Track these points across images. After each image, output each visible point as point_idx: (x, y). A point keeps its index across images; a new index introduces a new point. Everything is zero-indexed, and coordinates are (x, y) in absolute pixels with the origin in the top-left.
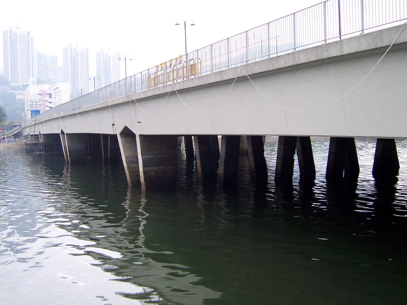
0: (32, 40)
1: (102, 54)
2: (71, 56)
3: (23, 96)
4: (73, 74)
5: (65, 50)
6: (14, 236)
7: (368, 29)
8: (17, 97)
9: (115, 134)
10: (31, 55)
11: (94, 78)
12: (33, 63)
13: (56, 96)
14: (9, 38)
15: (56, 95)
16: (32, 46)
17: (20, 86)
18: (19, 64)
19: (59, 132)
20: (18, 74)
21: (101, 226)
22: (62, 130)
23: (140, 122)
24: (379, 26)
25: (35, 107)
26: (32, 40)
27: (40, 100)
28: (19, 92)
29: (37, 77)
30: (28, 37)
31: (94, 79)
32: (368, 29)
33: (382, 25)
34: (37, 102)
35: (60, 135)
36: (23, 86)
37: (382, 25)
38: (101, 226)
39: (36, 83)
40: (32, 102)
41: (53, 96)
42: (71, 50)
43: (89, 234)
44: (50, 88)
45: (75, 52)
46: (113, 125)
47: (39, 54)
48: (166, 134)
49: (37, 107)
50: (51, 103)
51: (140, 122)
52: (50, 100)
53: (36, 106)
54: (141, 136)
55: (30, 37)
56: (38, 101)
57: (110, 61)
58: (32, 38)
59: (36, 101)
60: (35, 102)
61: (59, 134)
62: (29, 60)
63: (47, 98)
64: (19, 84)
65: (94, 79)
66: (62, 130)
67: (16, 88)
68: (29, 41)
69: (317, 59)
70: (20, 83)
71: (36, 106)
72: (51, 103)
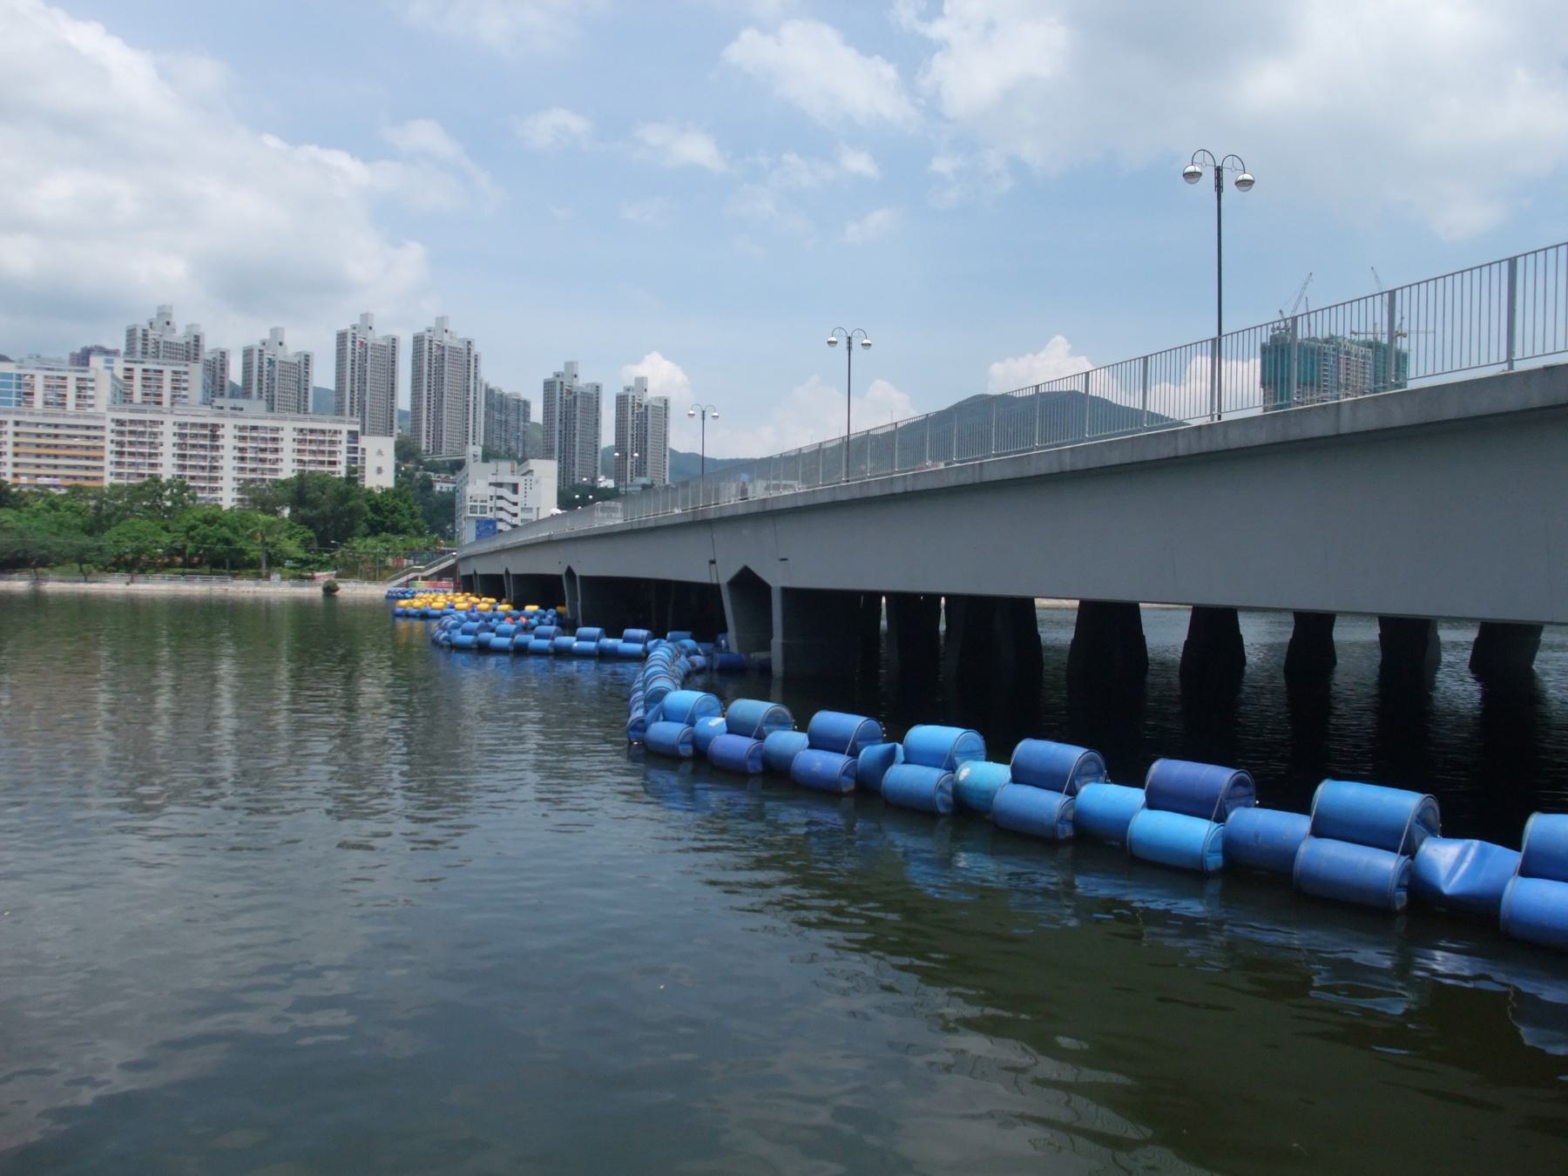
0: (476, 360)
3: (451, 486)
5: (549, 386)
7: (1446, 373)
8: (438, 488)
9: (715, 581)
10: (472, 395)
11: (849, 338)
12: (475, 412)
13: (528, 490)
15: (528, 487)
16: (476, 366)
19: (502, 572)
20: (441, 435)
21: (850, 941)
22: (507, 570)
23: (786, 559)
24: (1554, 355)
26: (476, 360)
28: (443, 476)
29: (482, 443)
30: (469, 353)
31: (849, 343)
32: (1446, 373)
33: (1430, 376)
34: (486, 502)
37: (1430, 376)
38: (850, 941)
39: (480, 458)
40: (475, 501)
41: (521, 489)
46: (713, 562)
47: (490, 392)
48: (1114, 598)
50: (515, 504)
51: (786, 559)
52: (514, 498)
54: (786, 592)
55: (473, 354)
56: (489, 498)
58: (476, 356)
59: (484, 499)
65: (849, 343)
66: (507, 570)
67: (436, 468)
68: (469, 361)
69: (1271, 441)
70: (446, 455)
72: (515, 504)
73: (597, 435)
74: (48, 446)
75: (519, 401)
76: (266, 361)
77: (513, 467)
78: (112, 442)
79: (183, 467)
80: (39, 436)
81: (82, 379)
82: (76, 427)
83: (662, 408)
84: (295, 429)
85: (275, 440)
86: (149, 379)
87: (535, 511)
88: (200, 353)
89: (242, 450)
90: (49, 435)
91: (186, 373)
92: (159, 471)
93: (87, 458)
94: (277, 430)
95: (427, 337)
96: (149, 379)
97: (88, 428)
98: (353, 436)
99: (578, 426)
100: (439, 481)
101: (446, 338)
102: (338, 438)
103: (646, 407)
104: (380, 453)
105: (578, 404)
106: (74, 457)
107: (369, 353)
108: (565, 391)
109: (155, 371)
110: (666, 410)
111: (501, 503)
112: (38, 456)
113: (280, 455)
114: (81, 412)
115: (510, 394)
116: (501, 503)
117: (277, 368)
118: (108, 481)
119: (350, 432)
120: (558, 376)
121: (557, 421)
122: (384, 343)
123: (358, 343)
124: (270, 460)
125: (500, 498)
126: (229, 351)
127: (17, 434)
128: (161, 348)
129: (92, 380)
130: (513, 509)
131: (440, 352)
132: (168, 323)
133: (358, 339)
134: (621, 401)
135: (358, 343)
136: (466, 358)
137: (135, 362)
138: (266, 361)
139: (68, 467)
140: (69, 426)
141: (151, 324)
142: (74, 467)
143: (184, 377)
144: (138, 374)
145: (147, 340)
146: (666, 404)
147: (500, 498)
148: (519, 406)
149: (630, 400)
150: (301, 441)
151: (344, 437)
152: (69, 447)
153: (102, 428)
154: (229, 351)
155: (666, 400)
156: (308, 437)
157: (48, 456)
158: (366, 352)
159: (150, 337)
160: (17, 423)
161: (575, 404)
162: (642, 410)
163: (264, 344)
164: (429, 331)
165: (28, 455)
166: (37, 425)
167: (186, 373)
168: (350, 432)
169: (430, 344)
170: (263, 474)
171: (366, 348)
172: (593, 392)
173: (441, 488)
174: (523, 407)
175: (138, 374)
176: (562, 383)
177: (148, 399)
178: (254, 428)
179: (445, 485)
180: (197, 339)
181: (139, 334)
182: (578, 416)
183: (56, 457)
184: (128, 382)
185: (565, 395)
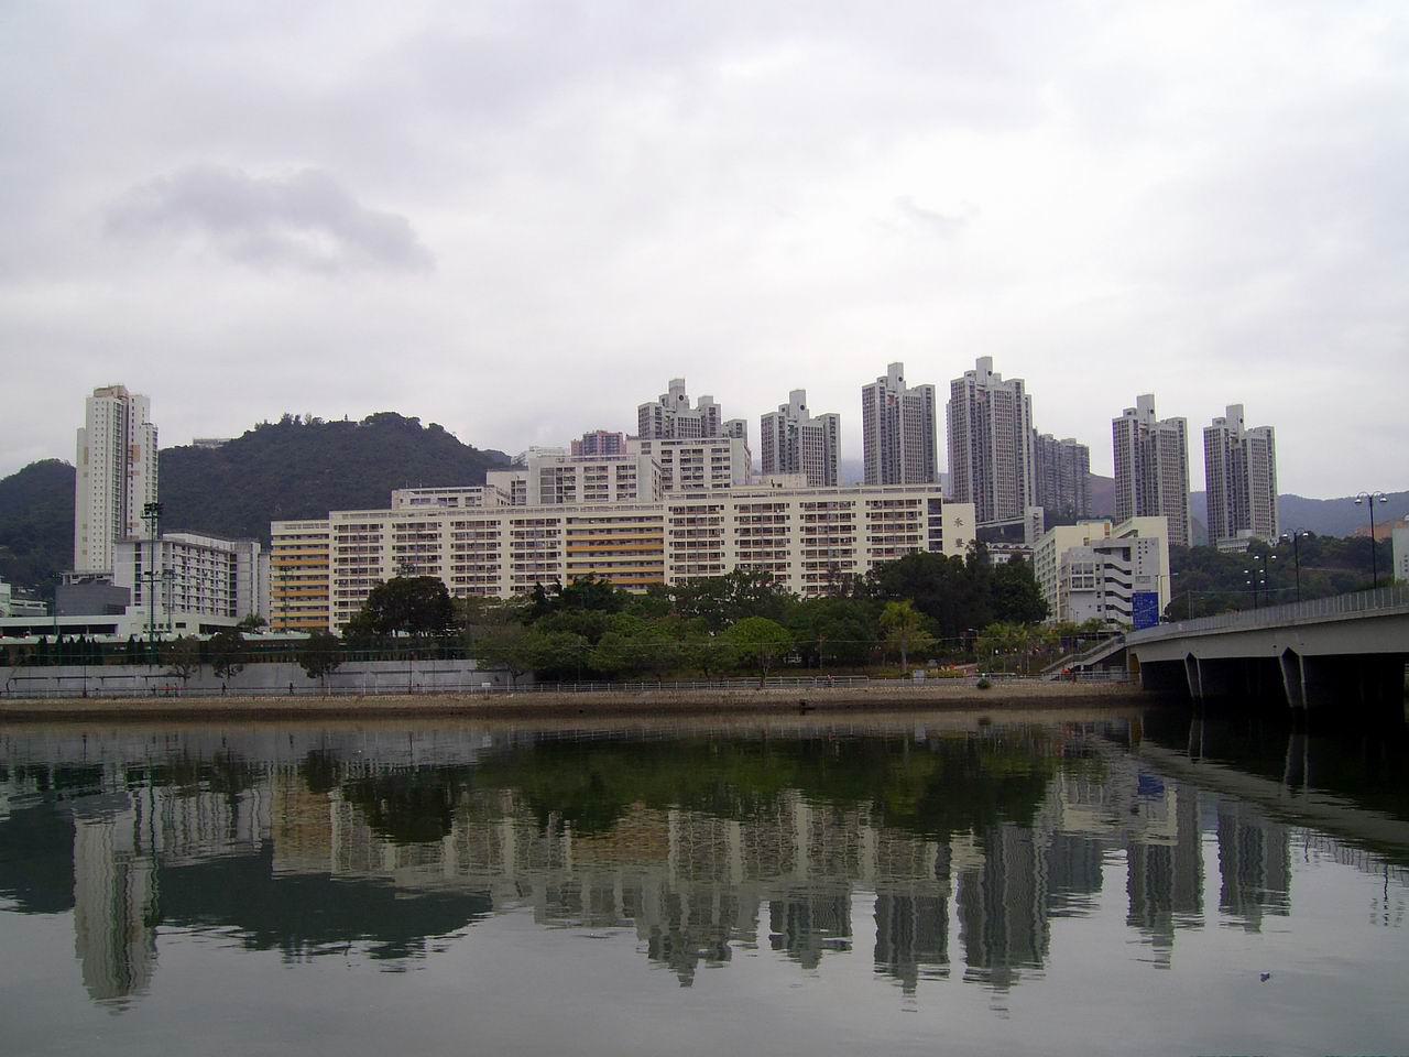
1: (1223, 435)
2: (1136, 444)
4: (888, 472)
5: (1119, 427)
6: (483, 917)
14: (968, 403)
17: (998, 529)
18: (994, 470)
20: (992, 497)
25: (1086, 586)
27: (1098, 566)
28: (1001, 545)
30: (1019, 397)
34: (1092, 572)
35: (1281, 662)
36: (1007, 528)
42: (1227, 435)
43: (1068, 909)
44: (1107, 534)
45: (1148, 432)
49: (1092, 586)
50: (1128, 573)
52: (1125, 566)
53: (1089, 583)
55: (1023, 398)
56: (1094, 568)
57: (1245, 454)
60: (1086, 573)
61: (1276, 659)
62: (1021, 459)
63: (1116, 559)
64: (995, 525)
68: (1019, 406)
71: (1089, 583)
72: (1128, 573)
73: (1184, 483)
74: (602, 542)
75: (1074, 448)
76: (787, 429)
77: (1107, 527)
78: (671, 532)
79: (745, 555)
80: (591, 532)
81: (624, 468)
82: (629, 519)
83: (1263, 441)
84: (867, 503)
85: (492, 535)
86: (689, 460)
87: (1153, 579)
88: (717, 426)
89: (810, 530)
90: (601, 531)
91: (727, 450)
92: (499, 594)
93: (641, 552)
94: (781, 506)
95: (967, 383)
96: (689, 460)
97: (641, 519)
98: (935, 505)
99: (1159, 472)
100: (997, 552)
101: (990, 381)
102: (919, 508)
103: (1244, 441)
104: (958, 522)
105: (1159, 446)
106: (629, 553)
107: (901, 408)
108: (1140, 431)
109: (694, 451)
110: (1270, 443)
111: (1110, 573)
112: (592, 554)
113: (853, 534)
114: (622, 503)
115: (1064, 441)
116: (1110, 573)
117: (800, 434)
118: (506, 594)
119: (930, 501)
120: (1129, 413)
121: (1133, 468)
122: (918, 395)
123: (887, 398)
124: (842, 540)
125: (1109, 566)
126: (746, 421)
127: (570, 532)
128: (676, 425)
129: (633, 467)
130: (1126, 579)
131: (984, 399)
132: (681, 398)
133: (887, 394)
134: (1210, 435)
135: (887, 398)
136: (1014, 400)
137: (674, 443)
138: (787, 429)
139: (622, 563)
140: (622, 519)
141: (663, 400)
142: (629, 563)
143: (724, 455)
144: (676, 456)
145: (660, 419)
146: (1269, 436)
147: (1109, 566)
148: (1075, 454)
149: (1223, 435)
150: (519, 545)
151: (924, 508)
152: (622, 542)
153: (327, 536)
154: (746, 421)
155: (1269, 431)
156: (883, 511)
157: (602, 553)
158: (898, 407)
159: (664, 415)
160: (569, 521)
161: (1154, 446)
162: (1240, 445)
163: (783, 410)
164: (1129, 413)
165: (582, 553)
166: (590, 520)
167: (727, 450)
168: (930, 501)
169: (972, 391)
170: (834, 556)
171: (897, 403)
172: (1176, 429)
173: (1001, 559)
174: (1079, 455)
175: (676, 456)
176: (1135, 421)
177: (688, 482)
178: (823, 505)
179: (1004, 556)
180: (713, 411)
181: (652, 413)
182: (1159, 460)
183: (610, 553)
184: (667, 465)
185: (1140, 436)
